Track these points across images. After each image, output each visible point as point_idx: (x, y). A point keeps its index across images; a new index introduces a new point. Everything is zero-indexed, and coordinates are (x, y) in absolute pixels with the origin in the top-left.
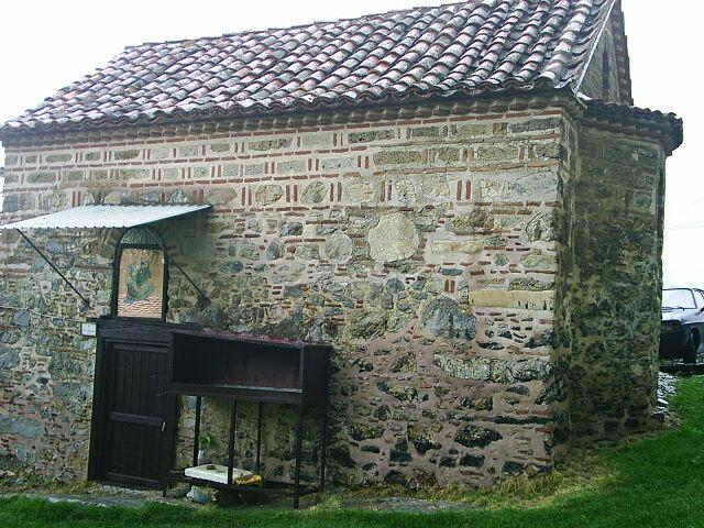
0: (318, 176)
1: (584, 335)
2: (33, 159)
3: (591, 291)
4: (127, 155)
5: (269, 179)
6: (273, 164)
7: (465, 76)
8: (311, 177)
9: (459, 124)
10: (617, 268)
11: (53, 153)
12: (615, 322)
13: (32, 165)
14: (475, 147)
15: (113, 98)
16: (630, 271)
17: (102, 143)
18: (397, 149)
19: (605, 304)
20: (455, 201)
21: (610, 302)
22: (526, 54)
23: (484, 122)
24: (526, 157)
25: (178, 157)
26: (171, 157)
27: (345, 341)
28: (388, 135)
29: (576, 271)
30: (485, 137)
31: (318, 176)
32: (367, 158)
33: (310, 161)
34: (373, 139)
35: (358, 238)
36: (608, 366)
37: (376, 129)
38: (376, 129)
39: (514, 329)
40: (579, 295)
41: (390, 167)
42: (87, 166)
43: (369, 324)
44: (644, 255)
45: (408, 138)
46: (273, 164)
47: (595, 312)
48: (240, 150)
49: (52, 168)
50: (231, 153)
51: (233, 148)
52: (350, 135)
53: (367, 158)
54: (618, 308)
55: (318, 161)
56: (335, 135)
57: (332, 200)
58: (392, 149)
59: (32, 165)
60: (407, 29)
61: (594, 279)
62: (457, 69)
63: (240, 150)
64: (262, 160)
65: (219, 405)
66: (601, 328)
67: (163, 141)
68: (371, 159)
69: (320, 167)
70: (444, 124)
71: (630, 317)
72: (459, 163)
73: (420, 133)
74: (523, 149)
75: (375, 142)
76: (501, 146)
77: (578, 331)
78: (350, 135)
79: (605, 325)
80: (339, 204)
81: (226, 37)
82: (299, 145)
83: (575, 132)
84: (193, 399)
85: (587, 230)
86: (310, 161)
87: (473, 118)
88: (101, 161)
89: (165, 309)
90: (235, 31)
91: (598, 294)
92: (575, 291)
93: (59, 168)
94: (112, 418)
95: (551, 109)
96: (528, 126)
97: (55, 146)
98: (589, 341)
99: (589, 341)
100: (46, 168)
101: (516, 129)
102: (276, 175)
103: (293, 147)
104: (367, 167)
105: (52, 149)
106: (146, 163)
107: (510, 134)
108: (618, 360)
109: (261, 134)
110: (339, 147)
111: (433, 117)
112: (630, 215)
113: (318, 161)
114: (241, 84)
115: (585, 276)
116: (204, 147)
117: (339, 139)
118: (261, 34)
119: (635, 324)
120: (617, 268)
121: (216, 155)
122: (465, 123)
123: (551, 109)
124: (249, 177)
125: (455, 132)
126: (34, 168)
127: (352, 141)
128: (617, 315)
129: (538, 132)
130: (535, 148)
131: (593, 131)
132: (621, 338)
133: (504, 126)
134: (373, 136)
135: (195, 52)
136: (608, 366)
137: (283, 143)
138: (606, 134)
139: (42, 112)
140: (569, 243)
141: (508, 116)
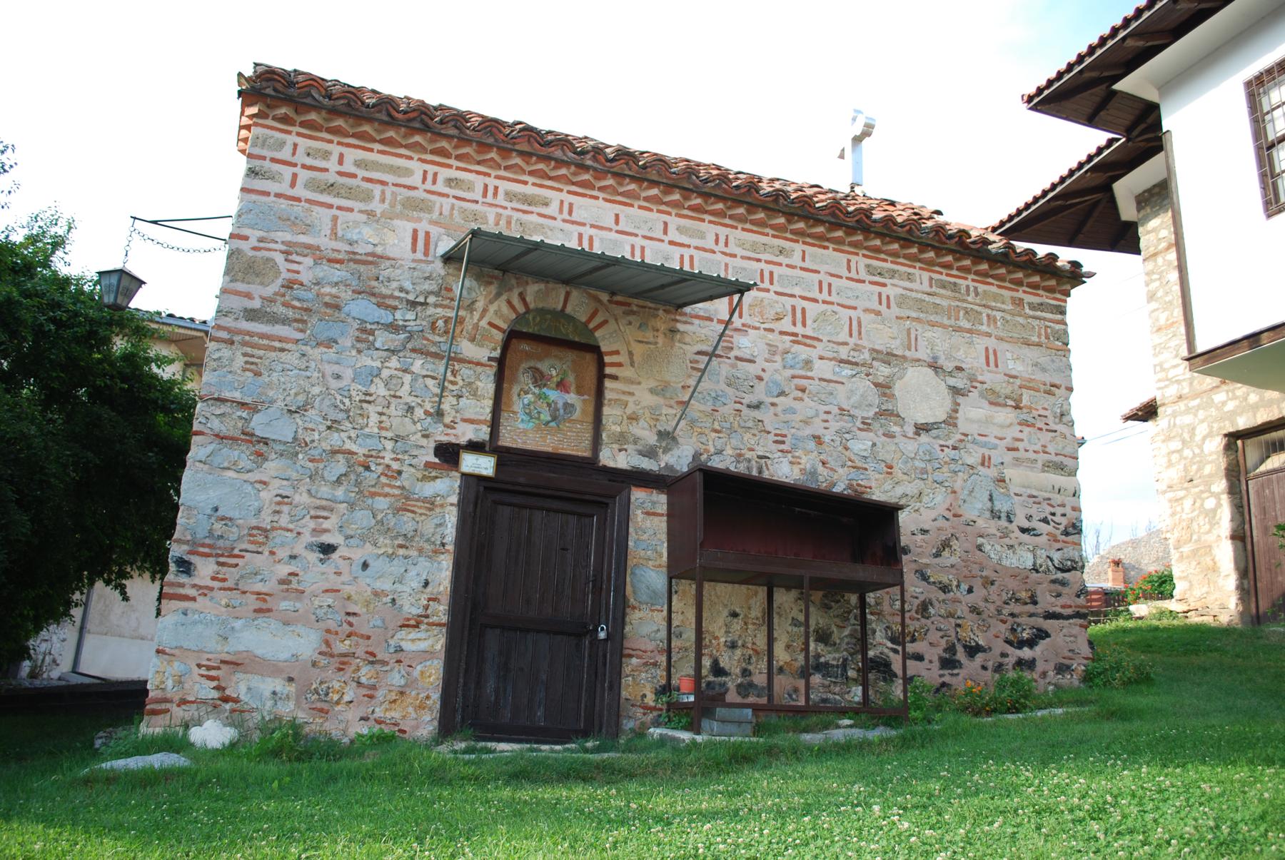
8: (824, 302)
14: (998, 315)
18: (919, 296)
23: (1003, 292)
30: (1003, 306)
34: (892, 277)
35: (884, 388)
73: (943, 285)
75: (895, 281)
117: (853, 265)
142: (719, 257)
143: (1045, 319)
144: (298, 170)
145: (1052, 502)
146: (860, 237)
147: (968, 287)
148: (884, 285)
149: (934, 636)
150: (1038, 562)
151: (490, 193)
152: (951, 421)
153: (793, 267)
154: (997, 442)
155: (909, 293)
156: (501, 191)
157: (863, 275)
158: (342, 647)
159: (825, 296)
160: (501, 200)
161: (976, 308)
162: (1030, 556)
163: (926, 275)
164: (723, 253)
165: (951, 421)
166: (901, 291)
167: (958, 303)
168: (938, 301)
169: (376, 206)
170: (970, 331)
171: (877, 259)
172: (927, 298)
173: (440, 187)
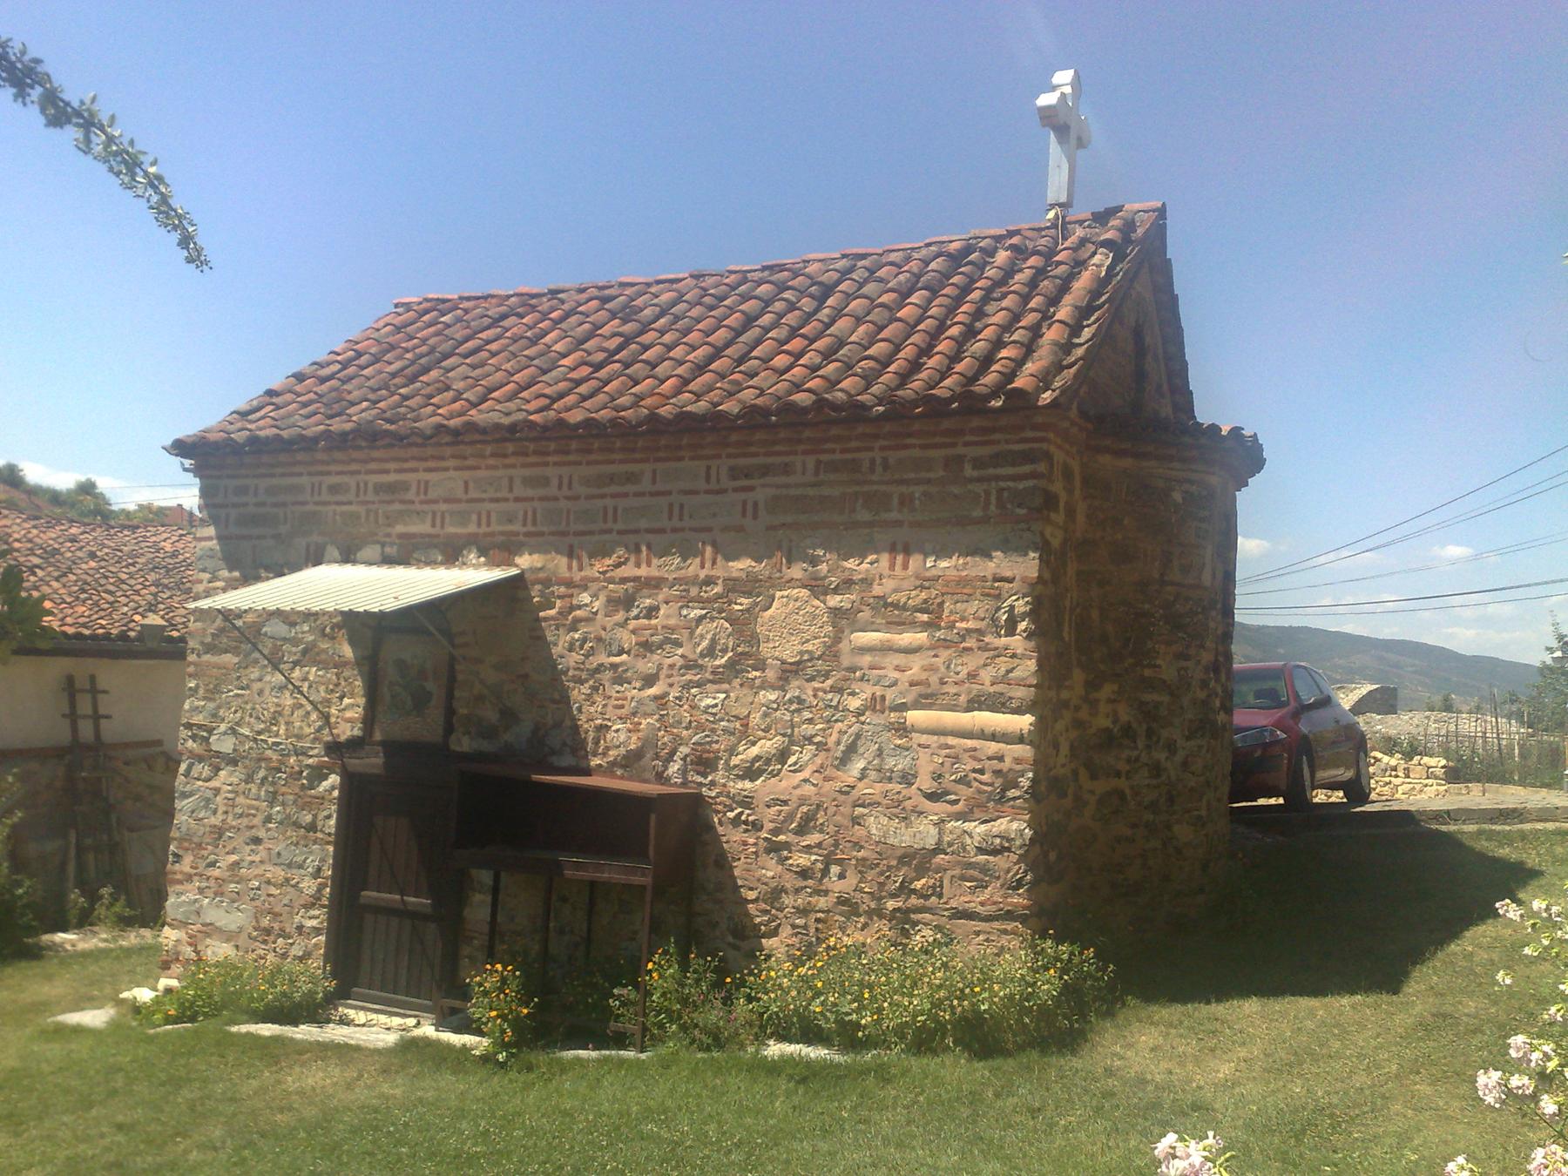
0: (682, 530)
1: (1094, 777)
2: (243, 490)
3: (1103, 708)
4: (391, 488)
5: (609, 531)
6: (615, 509)
7: (904, 378)
8: (674, 530)
9: (893, 456)
10: (1147, 672)
11: (275, 481)
12: (1144, 758)
13: (244, 499)
14: (918, 491)
15: (371, 396)
16: (1168, 672)
17: (354, 467)
18: (799, 492)
19: (1128, 731)
20: (886, 572)
21: (1135, 725)
22: (998, 344)
23: (932, 453)
24: (993, 507)
25: (473, 494)
26: (460, 493)
27: (721, 785)
28: (787, 469)
29: (1078, 676)
30: (932, 475)
31: (682, 530)
32: (756, 504)
33: (671, 505)
34: (764, 475)
35: (743, 625)
36: (1134, 826)
37: (770, 460)
38: (770, 460)
39: (974, 771)
40: (1083, 714)
41: (789, 519)
42: (328, 503)
43: (758, 758)
44: (1192, 651)
45: (817, 473)
46: (615, 509)
47: (1108, 740)
48: (565, 487)
49: (275, 505)
50: (553, 490)
51: (555, 482)
52: (732, 469)
53: (756, 504)
54: (1150, 733)
55: (682, 506)
56: (709, 468)
57: (703, 567)
58: (793, 492)
59: (244, 499)
60: (828, 290)
61: (1108, 690)
62: (954, 280)
63: (565, 487)
64: (600, 503)
65: (809, 402)
66: (1123, 766)
67: (446, 469)
68: (761, 506)
69: (686, 517)
70: (870, 454)
71: (1171, 748)
72: (894, 515)
73: (834, 467)
74: (987, 493)
75: (769, 480)
76: (956, 490)
77: (1083, 772)
78: (732, 469)
79: (1129, 761)
80: (713, 573)
81: (554, 293)
82: (654, 482)
83: (1075, 465)
84: (485, 877)
85: (1095, 614)
86: (671, 505)
87: (914, 446)
88: (351, 496)
89: (449, 729)
90: (567, 285)
91: (1115, 713)
92: (1077, 708)
93: (284, 504)
94: (362, 901)
95: (1030, 434)
96: (997, 459)
97: (279, 470)
98: (1102, 786)
99: (1102, 786)
100: (263, 504)
101: (978, 463)
102: (620, 526)
103: (646, 485)
104: (755, 517)
105: (272, 476)
106: (422, 502)
107: (969, 471)
108: (1151, 817)
109: (597, 462)
110: (713, 486)
111: (854, 444)
112: (1169, 588)
113: (682, 506)
114: (571, 380)
115: (1092, 685)
116: (511, 479)
117: (713, 472)
118: (607, 292)
119: (1179, 758)
120: (1147, 672)
121: (530, 492)
122: (902, 454)
123: (1030, 434)
124: (581, 527)
125: (886, 467)
126: (246, 505)
127: (734, 478)
128: (1148, 747)
129: (1010, 471)
130: (1006, 494)
131: (1106, 459)
132: (1154, 782)
133: (960, 459)
134: (765, 471)
135: (504, 317)
136: (1134, 826)
137: (631, 478)
138: (1127, 462)
139: (258, 415)
140: (1066, 635)
141: (966, 444)
142: (563, 504)
143: (998, 478)
144: (465, 497)
145: (977, 754)
146: (662, 411)
147: (873, 461)
148: (751, 489)
149: (786, 931)
150: (946, 839)
151: (565, 481)
152: (831, 652)
153: (642, 494)
154: (896, 675)
155: (784, 491)
156: (370, 486)
157: (726, 483)
158: (265, 922)
159: (676, 523)
160: (371, 496)
161: (883, 488)
162: (934, 831)
163: (811, 461)
164: (568, 498)
165: (831, 652)
166: (771, 492)
167: (857, 488)
168: (826, 491)
169: (283, 529)
170: (870, 524)
171: (745, 455)
172: (811, 492)
173: (325, 497)
